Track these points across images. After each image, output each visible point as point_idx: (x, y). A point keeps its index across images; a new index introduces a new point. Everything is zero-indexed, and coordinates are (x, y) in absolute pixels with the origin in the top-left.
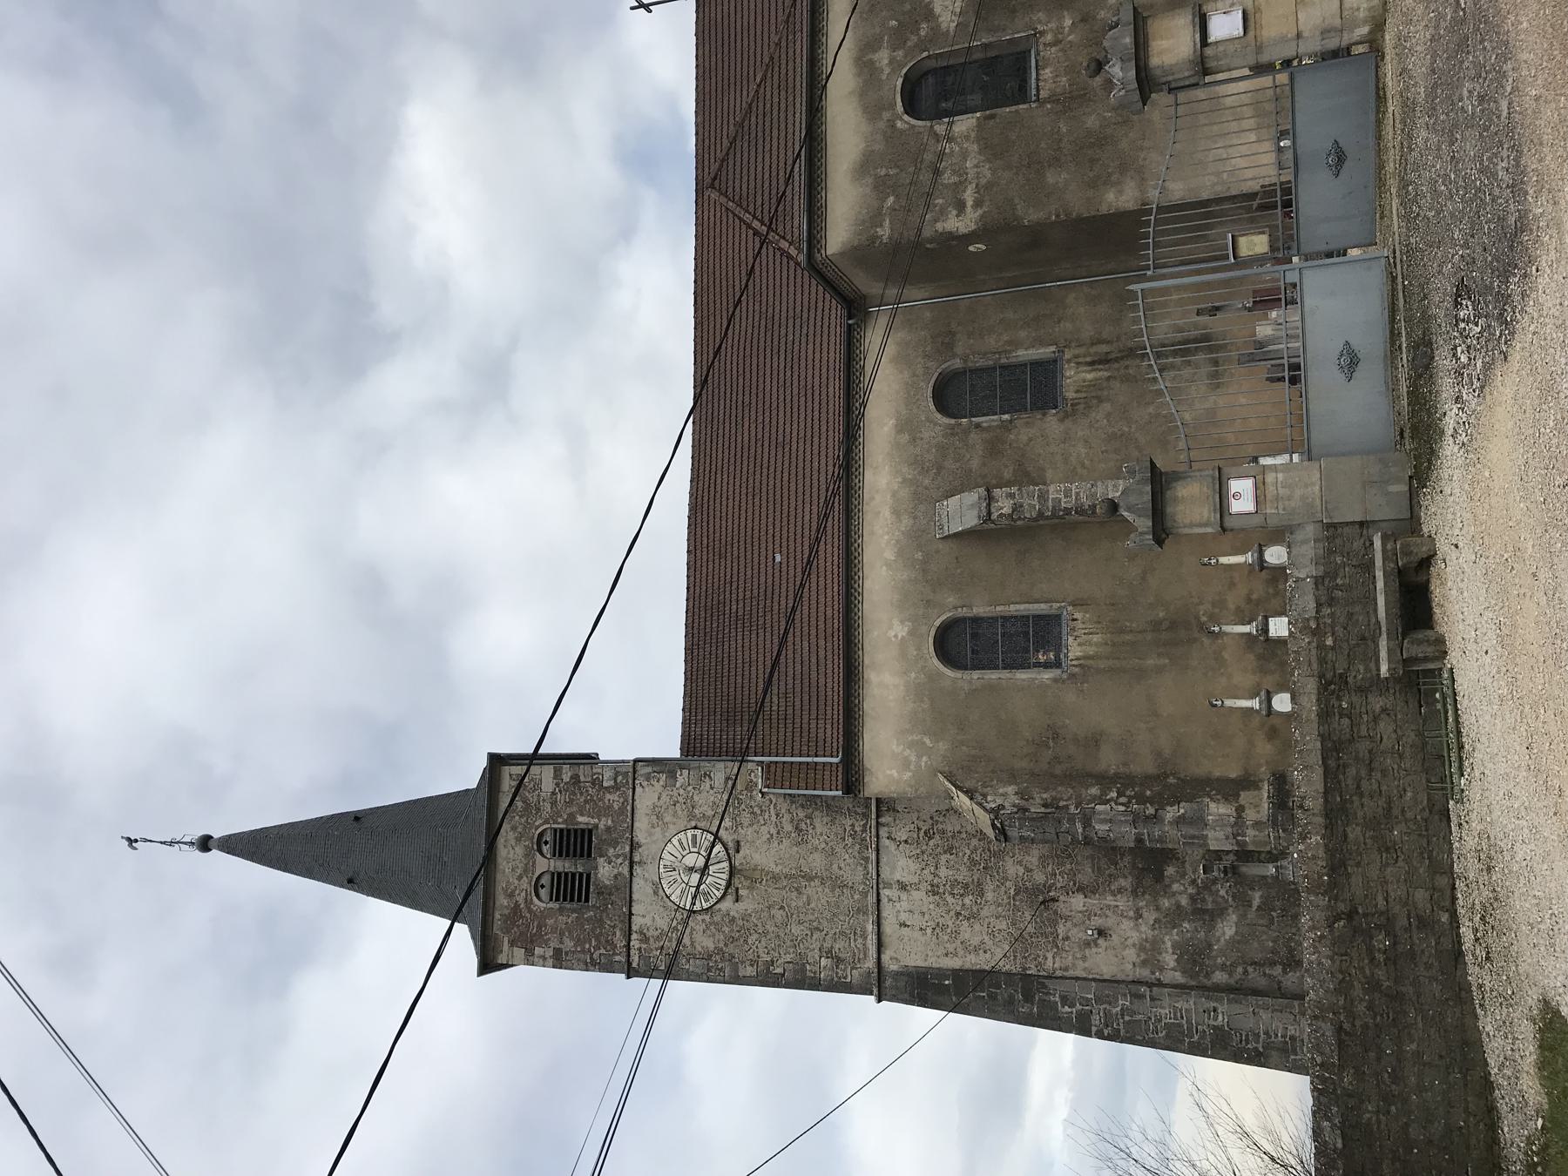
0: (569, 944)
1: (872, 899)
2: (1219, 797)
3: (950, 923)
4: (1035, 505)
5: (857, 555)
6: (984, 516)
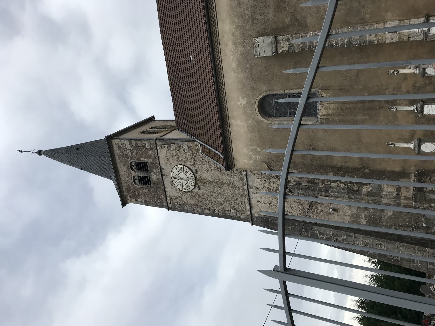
0: (148, 199)
1: (246, 192)
3: (276, 202)
4: (300, 45)
5: (219, 66)
6: (274, 52)
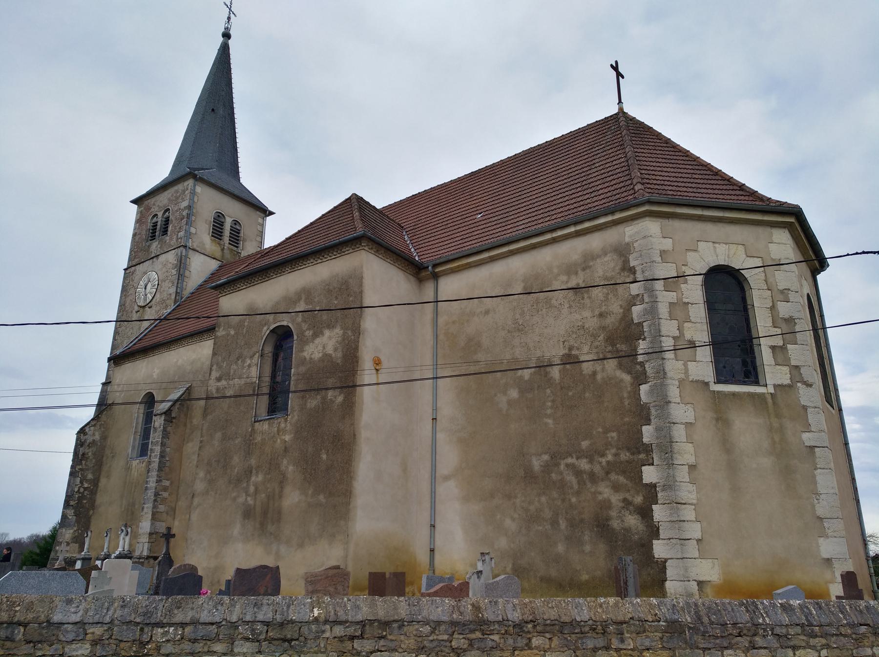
2: (76, 534)
